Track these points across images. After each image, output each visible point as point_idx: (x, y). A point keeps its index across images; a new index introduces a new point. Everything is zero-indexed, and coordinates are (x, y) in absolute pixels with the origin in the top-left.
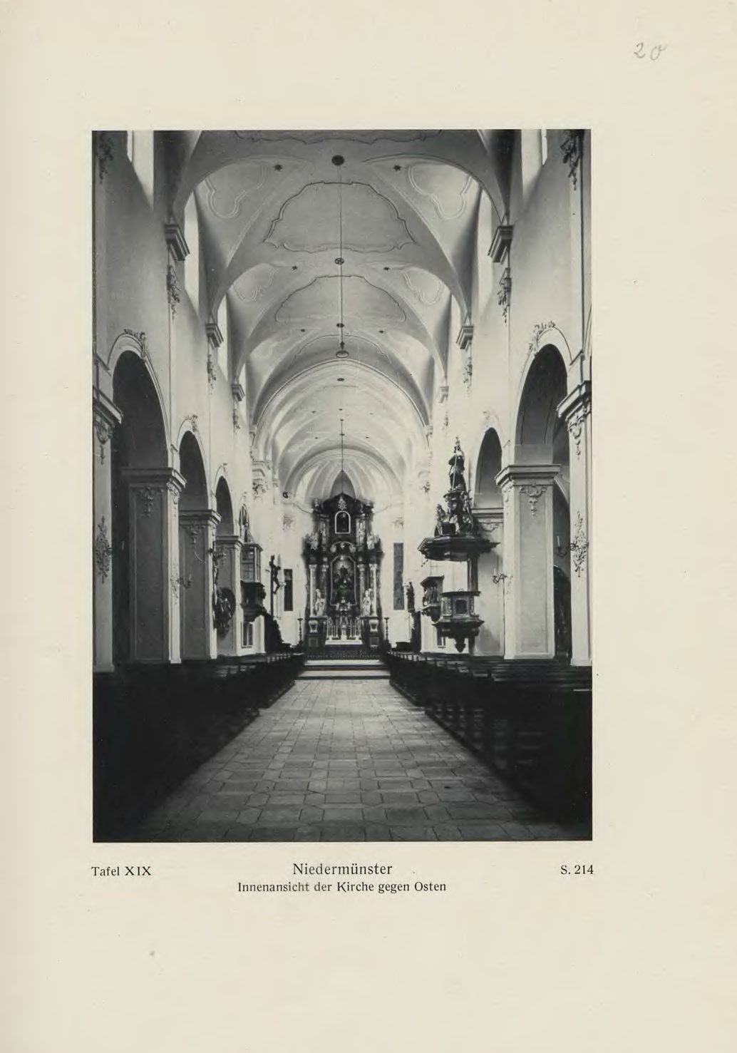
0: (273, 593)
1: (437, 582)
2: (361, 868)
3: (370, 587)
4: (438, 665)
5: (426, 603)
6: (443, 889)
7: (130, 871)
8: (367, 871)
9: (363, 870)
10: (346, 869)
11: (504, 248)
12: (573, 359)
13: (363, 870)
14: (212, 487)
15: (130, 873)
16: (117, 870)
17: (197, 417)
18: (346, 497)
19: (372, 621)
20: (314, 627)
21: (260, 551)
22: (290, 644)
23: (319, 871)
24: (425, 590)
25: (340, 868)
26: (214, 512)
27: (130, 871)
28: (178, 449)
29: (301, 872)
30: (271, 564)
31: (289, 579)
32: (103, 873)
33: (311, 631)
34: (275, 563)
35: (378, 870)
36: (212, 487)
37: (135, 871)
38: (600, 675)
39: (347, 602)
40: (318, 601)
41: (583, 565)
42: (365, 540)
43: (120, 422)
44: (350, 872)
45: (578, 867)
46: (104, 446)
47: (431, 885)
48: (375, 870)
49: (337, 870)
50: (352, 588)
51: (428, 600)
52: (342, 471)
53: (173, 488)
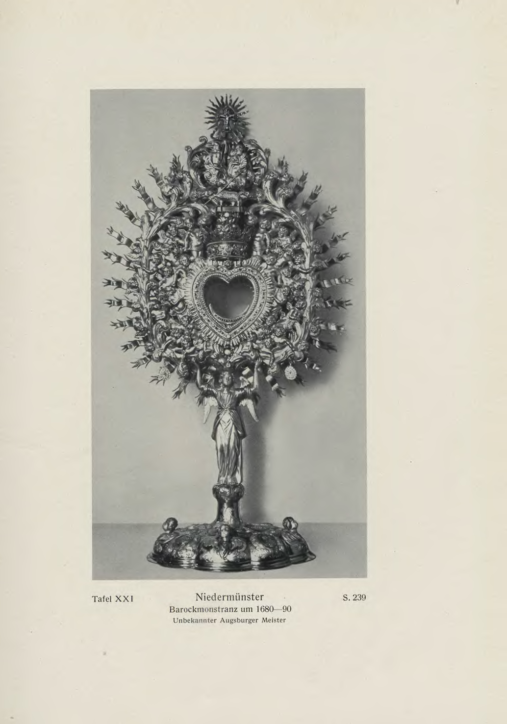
2: (242, 596)
4: (248, 193)
9: (244, 598)
13: (244, 598)
15: (118, 600)
16: (109, 598)
18: (314, 559)
23: (214, 599)
25: (228, 596)
32: (100, 600)
35: (254, 597)
37: (122, 599)
38: (412, 462)
44: (235, 599)
45: (355, 596)
48: (252, 597)
49: (226, 598)
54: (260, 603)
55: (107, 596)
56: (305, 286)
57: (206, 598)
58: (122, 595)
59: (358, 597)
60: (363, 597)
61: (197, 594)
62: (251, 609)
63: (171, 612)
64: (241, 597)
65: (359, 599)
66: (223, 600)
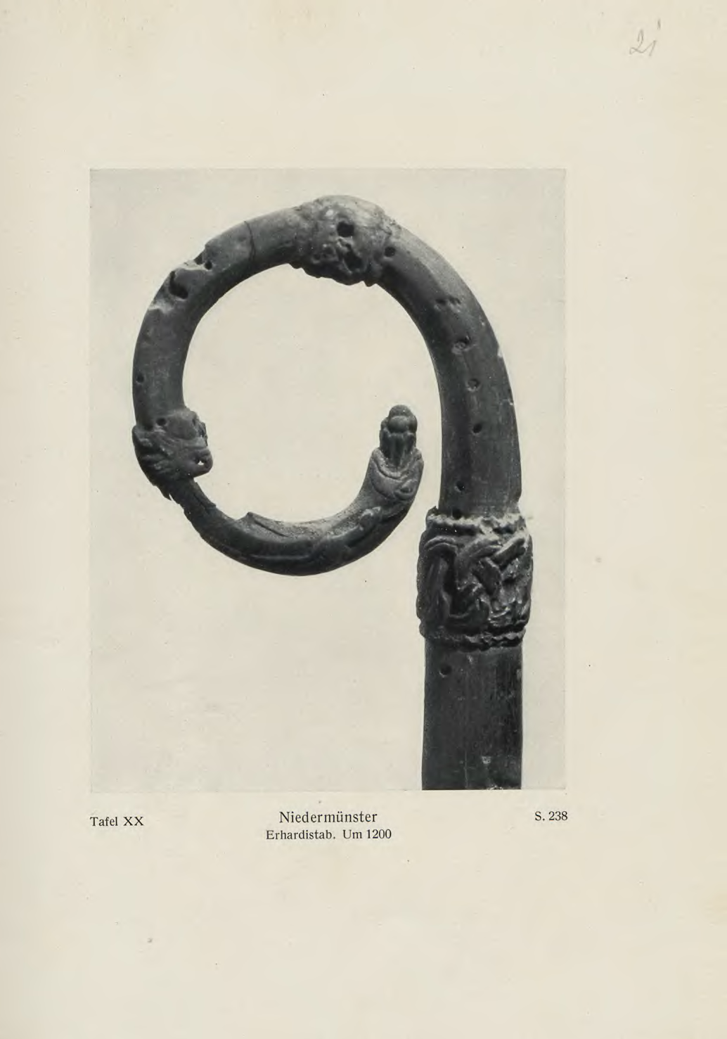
2: (346, 816)
6: (359, 837)
7: (128, 821)
8: (353, 818)
10: (332, 817)
11: (430, 566)
13: (349, 818)
23: (305, 820)
27: (139, 821)
29: (288, 820)
32: (102, 824)
37: (134, 821)
45: (552, 813)
47: (107, 820)
49: (322, 818)
54: (371, 826)
55: (112, 817)
56: (526, 627)
57: (294, 818)
58: (134, 816)
59: (556, 816)
60: (564, 816)
61: (282, 813)
62: (359, 834)
63: (268, 838)
64: (344, 817)
65: (558, 818)
66: (319, 821)
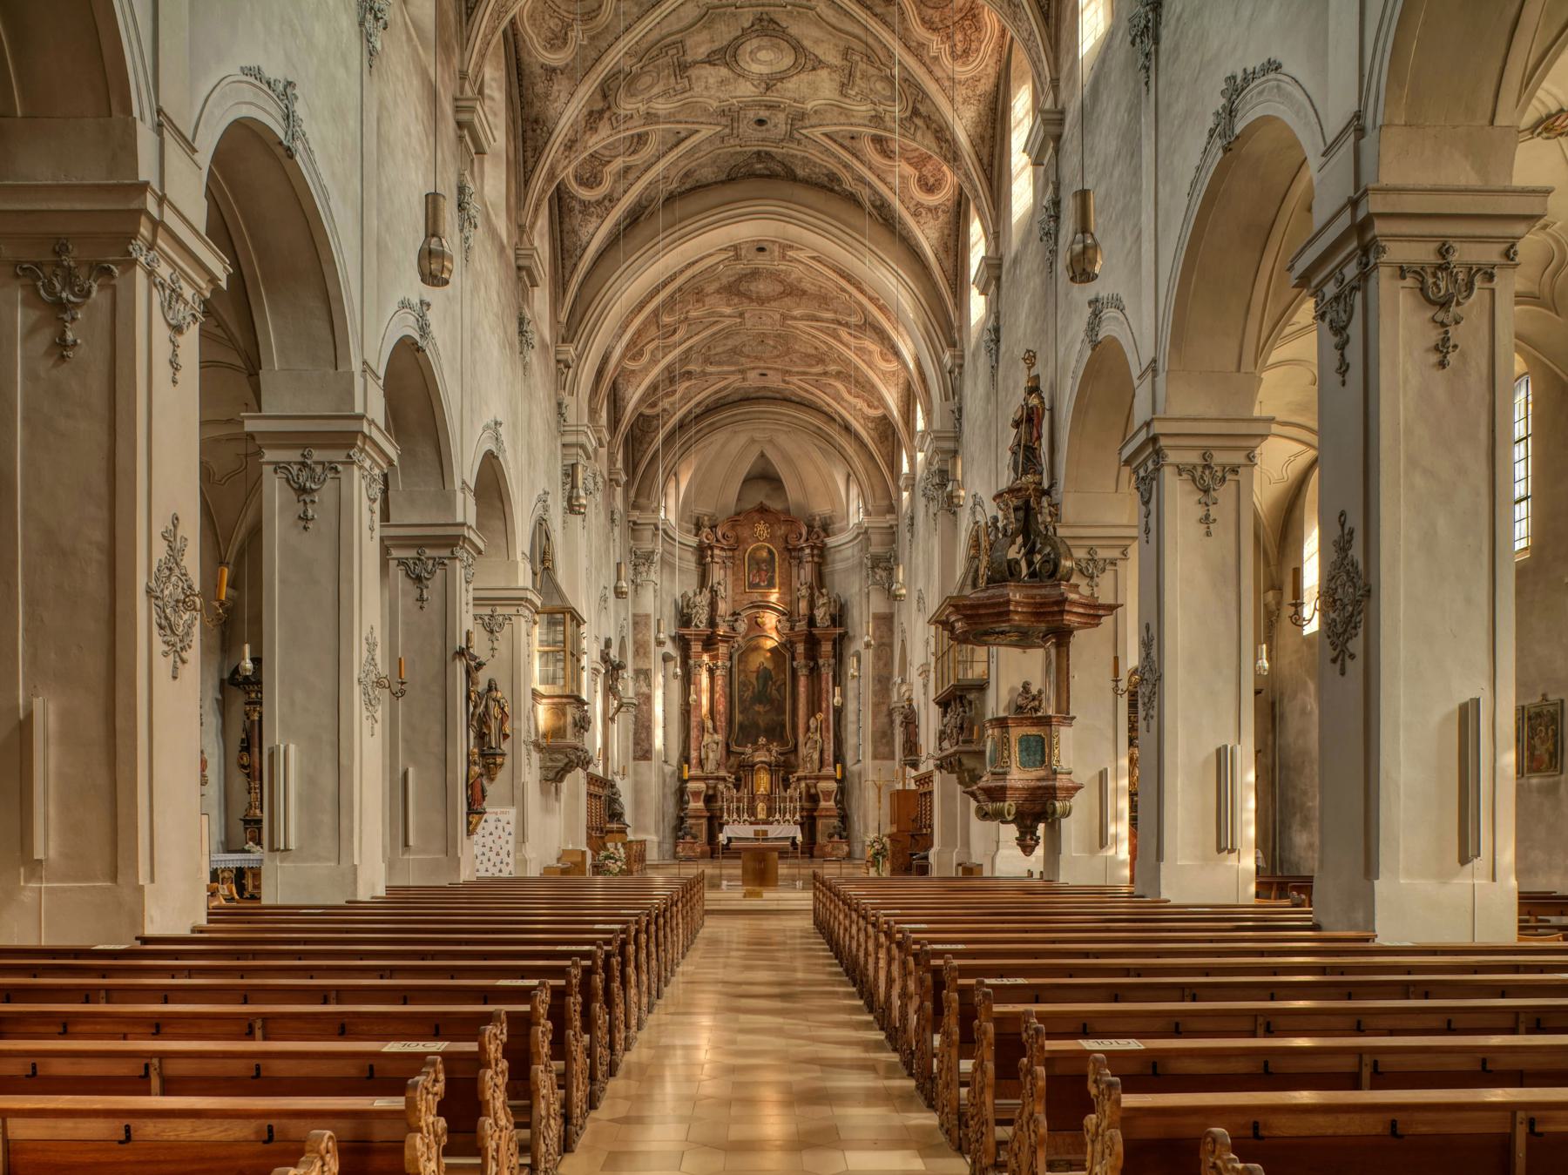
0: (608, 720)
1: (972, 696)
3: (820, 710)
5: (946, 744)
12: (1329, 142)
14: (466, 468)
17: (429, 305)
19: (822, 785)
20: (696, 794)
21: (578, 626)
22: (492, 780)
24: (944, 714)
26: (470, 527)
28: (382, 373)
30: (605, 658)
31: (645, 689)
33: (692, 805)
34: (614, 653)
36: (466, 468)
39: (769, 741)
40: (707, 738)
41: (1154, 713)
42: (812, 605)
43: (224, 284)
46: (180, 340)
50: (780, 710)
51: (950, 737)
52: (762, 455)
53: (367, 463)
